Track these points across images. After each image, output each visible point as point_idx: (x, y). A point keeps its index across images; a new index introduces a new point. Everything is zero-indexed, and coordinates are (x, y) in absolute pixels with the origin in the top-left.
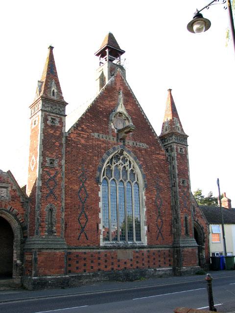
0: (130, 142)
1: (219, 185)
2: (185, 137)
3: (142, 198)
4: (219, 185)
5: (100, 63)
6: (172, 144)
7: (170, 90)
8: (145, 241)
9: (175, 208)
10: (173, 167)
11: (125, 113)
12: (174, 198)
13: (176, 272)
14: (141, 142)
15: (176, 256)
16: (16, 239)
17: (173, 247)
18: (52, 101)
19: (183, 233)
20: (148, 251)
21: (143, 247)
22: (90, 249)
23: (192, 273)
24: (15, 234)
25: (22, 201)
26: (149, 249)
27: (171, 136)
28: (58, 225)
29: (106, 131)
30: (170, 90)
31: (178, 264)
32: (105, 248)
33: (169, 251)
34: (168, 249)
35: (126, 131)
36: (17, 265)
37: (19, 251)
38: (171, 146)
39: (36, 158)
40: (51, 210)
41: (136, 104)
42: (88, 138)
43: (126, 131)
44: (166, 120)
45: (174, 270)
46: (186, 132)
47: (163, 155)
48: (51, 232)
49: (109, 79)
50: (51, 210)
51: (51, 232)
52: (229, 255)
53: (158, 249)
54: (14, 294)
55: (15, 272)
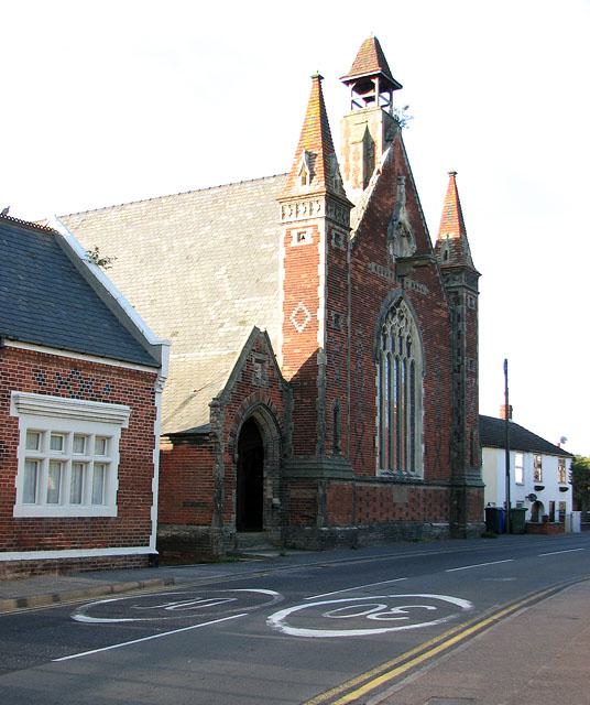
0: (409, 282)
1: (506, 372)
2: (474, 276)
3: (420, 391)
4: (506, 372)
5: (353, 102)
6: (459, 290)
7: (320, 78)
8: (420, 472)
9: (458, 412)
10: (459, 333)
11: (407, 223)
12: (457, 393)
13: (457, 532)
14: (421, 283)
15: (455, 502)
16: (270, 459)
17: (452, 486)
18: (337, 204)
19: (468, 462)
20: (424, 490)
21: (419, 483)
22: (366, 481)
23: (478, 535)
24: (270, 451)
25: (281, 389)
26: (426, 487)
27: (460, 273)
28: (344, 437)
29: (382, 258)
30: (320, 78)
31: (458, 518)
32: (382, 481)
33: (446, 491)
34: (445, 488)
35: (416, 262)
36: (273, 506)
37: (277, 482)
38: (457, 293)
39: (314, 310)
40: (336, 411)
41: (415, 204)
42: (365, 274)
43: (416, 262)
44: (445, 238)
45: (452, 527)
46: (478, 267)
47: (445, 309)
48: (336, 449)
49: (384, 149)
50: (336, 411)
51: (336, 449)
52: (514, 506)
53: (435, 488)
54: (297, 556)
55: (267, 517)
